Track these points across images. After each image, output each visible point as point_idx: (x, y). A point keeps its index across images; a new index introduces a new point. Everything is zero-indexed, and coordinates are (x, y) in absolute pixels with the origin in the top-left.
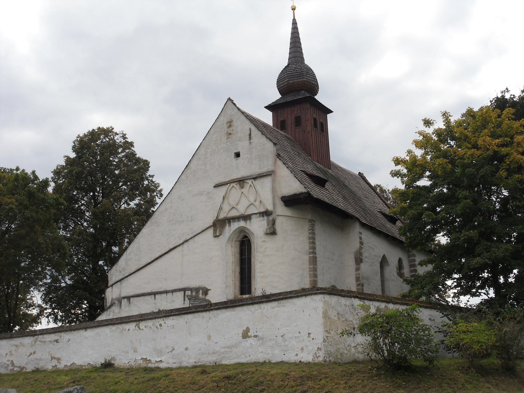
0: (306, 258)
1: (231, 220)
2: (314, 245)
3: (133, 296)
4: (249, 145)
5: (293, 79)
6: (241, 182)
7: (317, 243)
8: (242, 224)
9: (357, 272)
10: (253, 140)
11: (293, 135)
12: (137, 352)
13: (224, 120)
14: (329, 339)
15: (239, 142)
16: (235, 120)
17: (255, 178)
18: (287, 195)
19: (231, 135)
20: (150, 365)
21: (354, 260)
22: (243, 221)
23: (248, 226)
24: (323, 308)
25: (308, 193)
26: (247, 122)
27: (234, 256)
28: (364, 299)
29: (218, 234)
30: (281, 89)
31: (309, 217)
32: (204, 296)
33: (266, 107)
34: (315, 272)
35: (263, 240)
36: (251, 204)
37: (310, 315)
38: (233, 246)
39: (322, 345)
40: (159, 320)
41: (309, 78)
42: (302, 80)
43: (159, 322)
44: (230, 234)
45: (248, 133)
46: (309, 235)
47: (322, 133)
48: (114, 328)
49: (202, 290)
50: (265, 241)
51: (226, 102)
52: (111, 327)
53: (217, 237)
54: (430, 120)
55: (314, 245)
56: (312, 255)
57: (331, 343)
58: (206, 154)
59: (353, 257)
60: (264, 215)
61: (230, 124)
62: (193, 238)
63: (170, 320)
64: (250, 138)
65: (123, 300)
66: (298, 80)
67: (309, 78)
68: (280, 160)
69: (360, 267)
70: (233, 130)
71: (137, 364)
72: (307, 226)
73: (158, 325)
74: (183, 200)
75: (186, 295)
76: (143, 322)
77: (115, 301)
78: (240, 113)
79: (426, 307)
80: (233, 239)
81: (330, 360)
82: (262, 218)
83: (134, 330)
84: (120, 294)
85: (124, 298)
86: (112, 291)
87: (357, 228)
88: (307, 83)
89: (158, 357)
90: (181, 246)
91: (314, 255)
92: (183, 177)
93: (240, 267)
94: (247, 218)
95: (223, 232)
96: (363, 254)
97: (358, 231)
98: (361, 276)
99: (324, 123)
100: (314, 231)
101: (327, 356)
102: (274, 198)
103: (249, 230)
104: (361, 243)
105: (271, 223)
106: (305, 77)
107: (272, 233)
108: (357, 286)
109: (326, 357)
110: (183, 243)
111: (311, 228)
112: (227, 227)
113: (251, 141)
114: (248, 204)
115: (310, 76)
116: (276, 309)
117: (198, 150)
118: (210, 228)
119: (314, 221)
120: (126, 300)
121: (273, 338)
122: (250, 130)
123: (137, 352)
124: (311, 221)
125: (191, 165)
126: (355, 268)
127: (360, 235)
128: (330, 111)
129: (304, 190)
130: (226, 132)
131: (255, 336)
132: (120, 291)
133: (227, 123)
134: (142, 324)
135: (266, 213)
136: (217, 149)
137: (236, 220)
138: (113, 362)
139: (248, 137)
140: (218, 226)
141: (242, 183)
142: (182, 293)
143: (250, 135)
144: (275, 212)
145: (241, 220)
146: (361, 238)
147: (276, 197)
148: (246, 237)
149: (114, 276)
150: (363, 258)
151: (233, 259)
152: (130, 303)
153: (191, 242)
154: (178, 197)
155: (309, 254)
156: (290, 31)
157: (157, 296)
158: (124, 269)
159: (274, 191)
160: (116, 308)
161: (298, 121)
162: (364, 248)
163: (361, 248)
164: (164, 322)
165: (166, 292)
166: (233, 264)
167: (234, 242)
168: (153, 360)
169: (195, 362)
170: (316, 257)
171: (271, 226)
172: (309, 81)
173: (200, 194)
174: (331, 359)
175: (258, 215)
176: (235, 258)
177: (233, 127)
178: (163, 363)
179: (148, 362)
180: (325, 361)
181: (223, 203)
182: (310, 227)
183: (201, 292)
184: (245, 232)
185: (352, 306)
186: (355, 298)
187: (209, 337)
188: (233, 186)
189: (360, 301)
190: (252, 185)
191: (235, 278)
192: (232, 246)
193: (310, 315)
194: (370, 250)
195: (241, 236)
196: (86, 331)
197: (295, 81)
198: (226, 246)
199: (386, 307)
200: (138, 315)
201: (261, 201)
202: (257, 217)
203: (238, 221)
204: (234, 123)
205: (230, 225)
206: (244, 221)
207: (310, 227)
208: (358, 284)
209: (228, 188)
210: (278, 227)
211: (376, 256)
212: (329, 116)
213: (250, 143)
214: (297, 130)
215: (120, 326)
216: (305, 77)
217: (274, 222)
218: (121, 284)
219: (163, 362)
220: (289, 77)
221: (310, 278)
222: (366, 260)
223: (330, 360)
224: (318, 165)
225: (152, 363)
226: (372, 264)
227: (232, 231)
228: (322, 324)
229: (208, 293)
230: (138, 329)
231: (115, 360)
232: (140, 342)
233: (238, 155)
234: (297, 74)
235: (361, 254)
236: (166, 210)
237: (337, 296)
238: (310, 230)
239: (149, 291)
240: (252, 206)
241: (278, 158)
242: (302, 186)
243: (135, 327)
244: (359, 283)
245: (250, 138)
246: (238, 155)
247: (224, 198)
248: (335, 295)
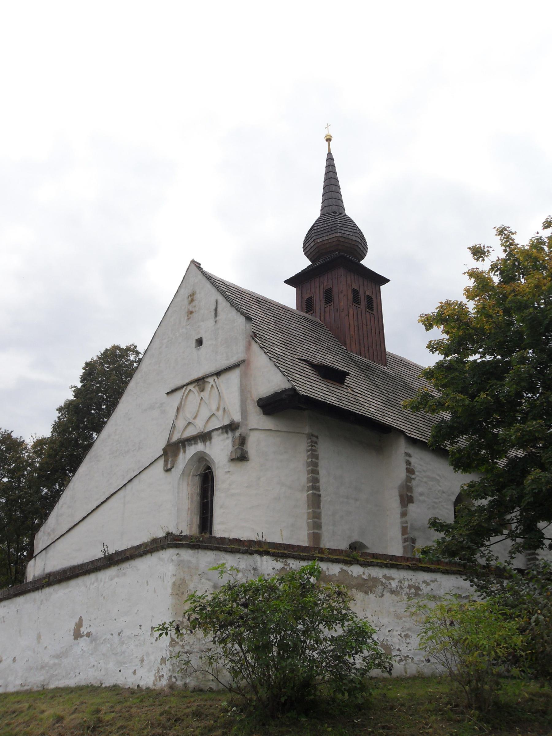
0: (303, 497)
1: (186, 443)
2: (316, 476)
4: (214, 325)
5: (322, 235)
7: (322, 472)
8: (200, 447)
9: (404, 519)
11: (322, 318)
13: (186, 293)
14: (186, 639)
15: (202, 323)
16: (197, 292)
17: (218, 374)
18: (268, 395)
19: (193, 314)
21: (398, 498)
22: (201, 442)
23: (207, 451)
24: (174, 575)
25: (293, 389)
26: (213, 291)
27: (190, 499)
28: (284, 556)
29: (169, 467)
30: (309, 253)
31: (307, 430)
33: (287, 282)
35: (227, 470)
37: (155, 591)
38: (190, 483)
39: (168, 652)
41: (346, 232)
42: (334, 235)
44: (184, 465)
45: (214, 307)
47: (370, 311)
50: (229, 472)
54: (482, 246)
55: (316, 476)
56: (311, 492)
57: (191, 647)
58: (160, 348)
59: (397, 494)
60: (228, 429)
61: (192, 298)
64: (216, 315)
66: (329, 237)
67: (346, 232)
68: (256, 342)
69: (407, 510)
70: (195, 307)
72: (303, 445)
78: (204, 280)
79: (446, 572)
80: (190, 472)
81: (185, 684)
82: (225, 436)
84: (44, 569)
86: (35, 564)
87: (402, 447)
88: (343, 240)
91: (314, 492)
93: (200, 517)
94: (205, 437)
95: (175, 463)
96: (414, 489)
97: (403, 452)
98: (409, 525)
99: (374, 299)
100: (316, 453)
101: (176, 675)
102: (243, 403)
103: (209, 456)
104: (410, 471)
105: (237, 442)
106: (339, 231)
108: (404, 543)
109: (175, 677)
111: (310, 447)
112: (181, 455)
113: (217, 318)
114: (209, 415)
115: (348, 229)
116: (116, 580)
117: (152, 343)
119: (317, 437)
121: (108, 637)
122: (217, 302)
124: (310, 436)
126: (399, 512)
127: (408, 458)
128: (385, 281)
129: (287, 386)
130: (186, 310)
132: (45, 564)
135: (231, 427)
136: (174, 338)
137: (193, 442)
139: (213, 313)
140: (169, 454)
141: (200, 383)
143: (216, 310)
144: (247, 425)
145: (199, 441)
146: (408, 463)
147: (249, 401)
148: (209, 468)
149: (41, 542)
150: (415, 495)
151: (189, 504)
153: (135, 481)
155: (308, 491)
156: (323, 170)
158: (53, 530)
159: (244, 391)
161: (329, 297)
162: (417, 478)
163: (409, 479)
166: (189, 512)
167: (191, 477)
170: (319, 496)
171: (237, 447)
172: (345, 236)
174: (188, 681)
175: (220, 430)
176: (192, 502)
177: (196, 302)
180: (172, 687)
181: (177, 417)
182: (309, 446)
184: (206, 460)
185: (252, 572)
186: (262, 556)
187: (39, 637)
188: (190, 390)
189: (276, 560)
190: (214, 385)
192: (188, 485)
193: (155, 591)
194: (431, 483)
195: (201, 468)
197: (324, 238)
198: (179, 484)
199: (342, 571)
202: (219, 435)
203: (195, 444)
204: (198, 296)
206: (202, 443)
207: (309, 446)
208: (405, 538)
209: (184, 394)
210: (251, 447)
211: (444, 492)
212: (383, 288)
213: (216, 322)
214: (327, 309)
216: (339, 231)
217: (243, 441)
218: (46, 553)
220: (316, 234)
221: (308, 531)
222: (421, 498)
223: (185, 684)
224: (357, 357)
226: (436, 506)
227: (187, 461)
228: (171, 609)
233: (200, 342)
234: (327, 228)
235: (410, 489)
236: (109, 436)
237: (215, 552)
240: (213, 419)
241: (253, 339)
242: (285, 379)
244: (406, 536)
245: (216, 315)
246: (200, 342)
247: (178, 409)
248: (212, 549)
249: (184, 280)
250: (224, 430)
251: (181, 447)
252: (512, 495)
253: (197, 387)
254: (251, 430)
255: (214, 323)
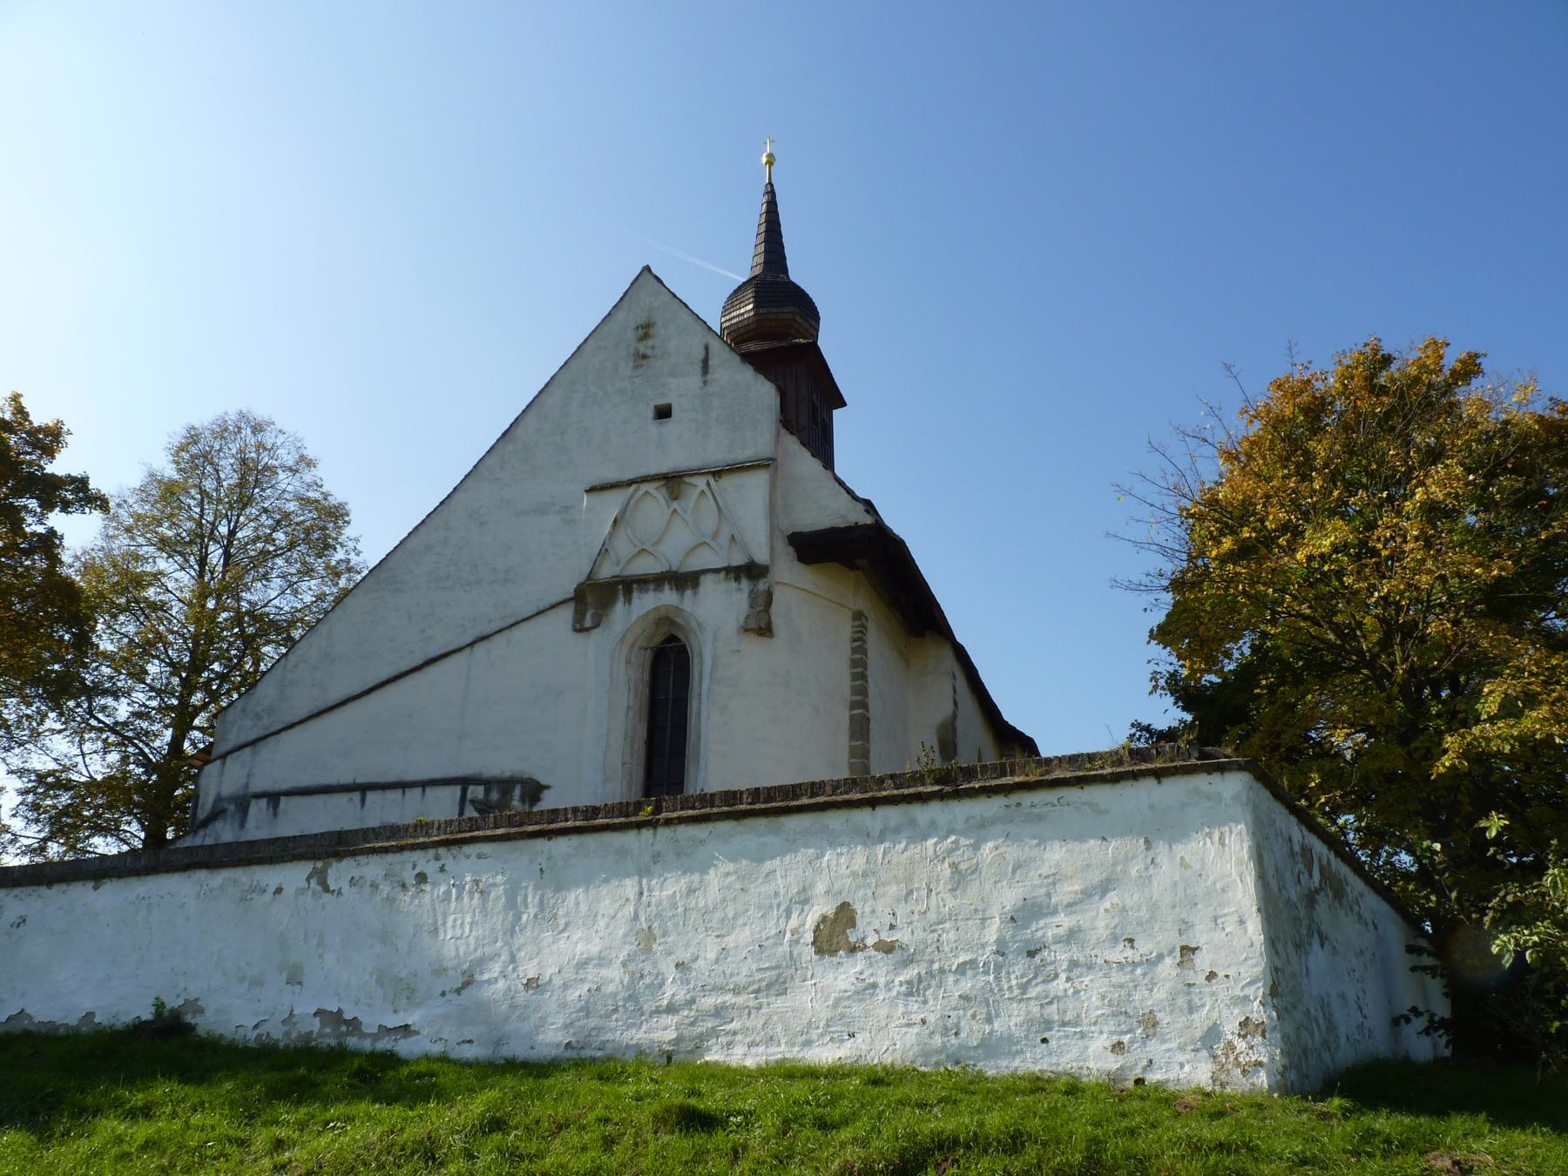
0: (843, 717)
1: (635, 586)
3: (290, 793)
6: (673, 482)
8: (668, 597)
10: (714, 376)
12: (300, 983)
17: (717, 474)
18: (806, 530)
20: (352, 1042)
22: (671, 589)
32: (527, 806)
34: (866, 761)
36: (701, 544)
38: (633, 661)
40: (416, 856)
43: (414, 867)
45: (701, 354)
46: (853, 654)
48: (218, 878)
49: (523, 788)
50: (738, 651)
51: (638, 277)
52: (201, 875)
53: (585, 634)
60: (742, 575)
62: (507, 632)
63: (468, 857)
65: (253, 802)
71: (294, 1035)
73: (409, 877)
74: (482, 524)
75: (469, 796)
76: (345, 861)
77: (226, 806)
82: (734, 585)
83: (301, 892)
85: (258, 796)
86: (222, 773)
89: (395, 1011)
90: (467, 652)
92: (489, 461)
94: (685, 580)
95: (604, 619)
105: (761, 601)
107: (760, 626)
110: (471, 644)
111: (859, 635)
112: (620, 606)
113: (709, 377)
117: (543, 396)
118: (564, 606)
120: (263, 802)
122: (707, 348)
123: (300, 983)
125: (520, 431)
130: (632, 349)
131: (887, 948)
132: (248, 775)
133: (637, 328)
134: (341, 872)
135: (751, 571)
138: (189, 1018)
139: (698, 368)
140: (589, 599)
142: (457, 790)
145: (667, 587)
148: (672, 638)
152: (275, 815)
153: (499, 640)
154: (470, 516)
157: (372, 797)
160: (228, 826)
164: (439, 864)
165: (403, 786)
166: (630, 714)
168: (370, 1023)
169: (569, 1044)
171: (761, 608)
173: (541, 510)
175: (722, 575)
178: (413, 1039)
179: (344, 1028)
182: (856, 632)
183: (517, 791)
188: (647, 492)
191: (632, 755)
192: (628, 662)
196: (96, 888)
200: (322, 834)
201: (733, 537)
203: (655, 590)
204: (659, 330)
205: (629, 600)
206: (674, 592)
207: (856, 632)
213: (705, 383)
215: (242, 875)
218: (287, 660)
219: (417, 1033)
225: (363, 1036)
227: (634, 618)
229: (542, 796)
230: (319, 888)
231: (201, 1011)
232: (321, 943)
236: (428, 548)
238: (854, 640)
239: (347, 779)
243: (308, 880)
247: (615, 521)
249: (627, 297)
250: (732, 575)
251: (621, 592)
252: (105, 753)
253: (664, 490)
254: (777, 583)
255: (702, 384)
